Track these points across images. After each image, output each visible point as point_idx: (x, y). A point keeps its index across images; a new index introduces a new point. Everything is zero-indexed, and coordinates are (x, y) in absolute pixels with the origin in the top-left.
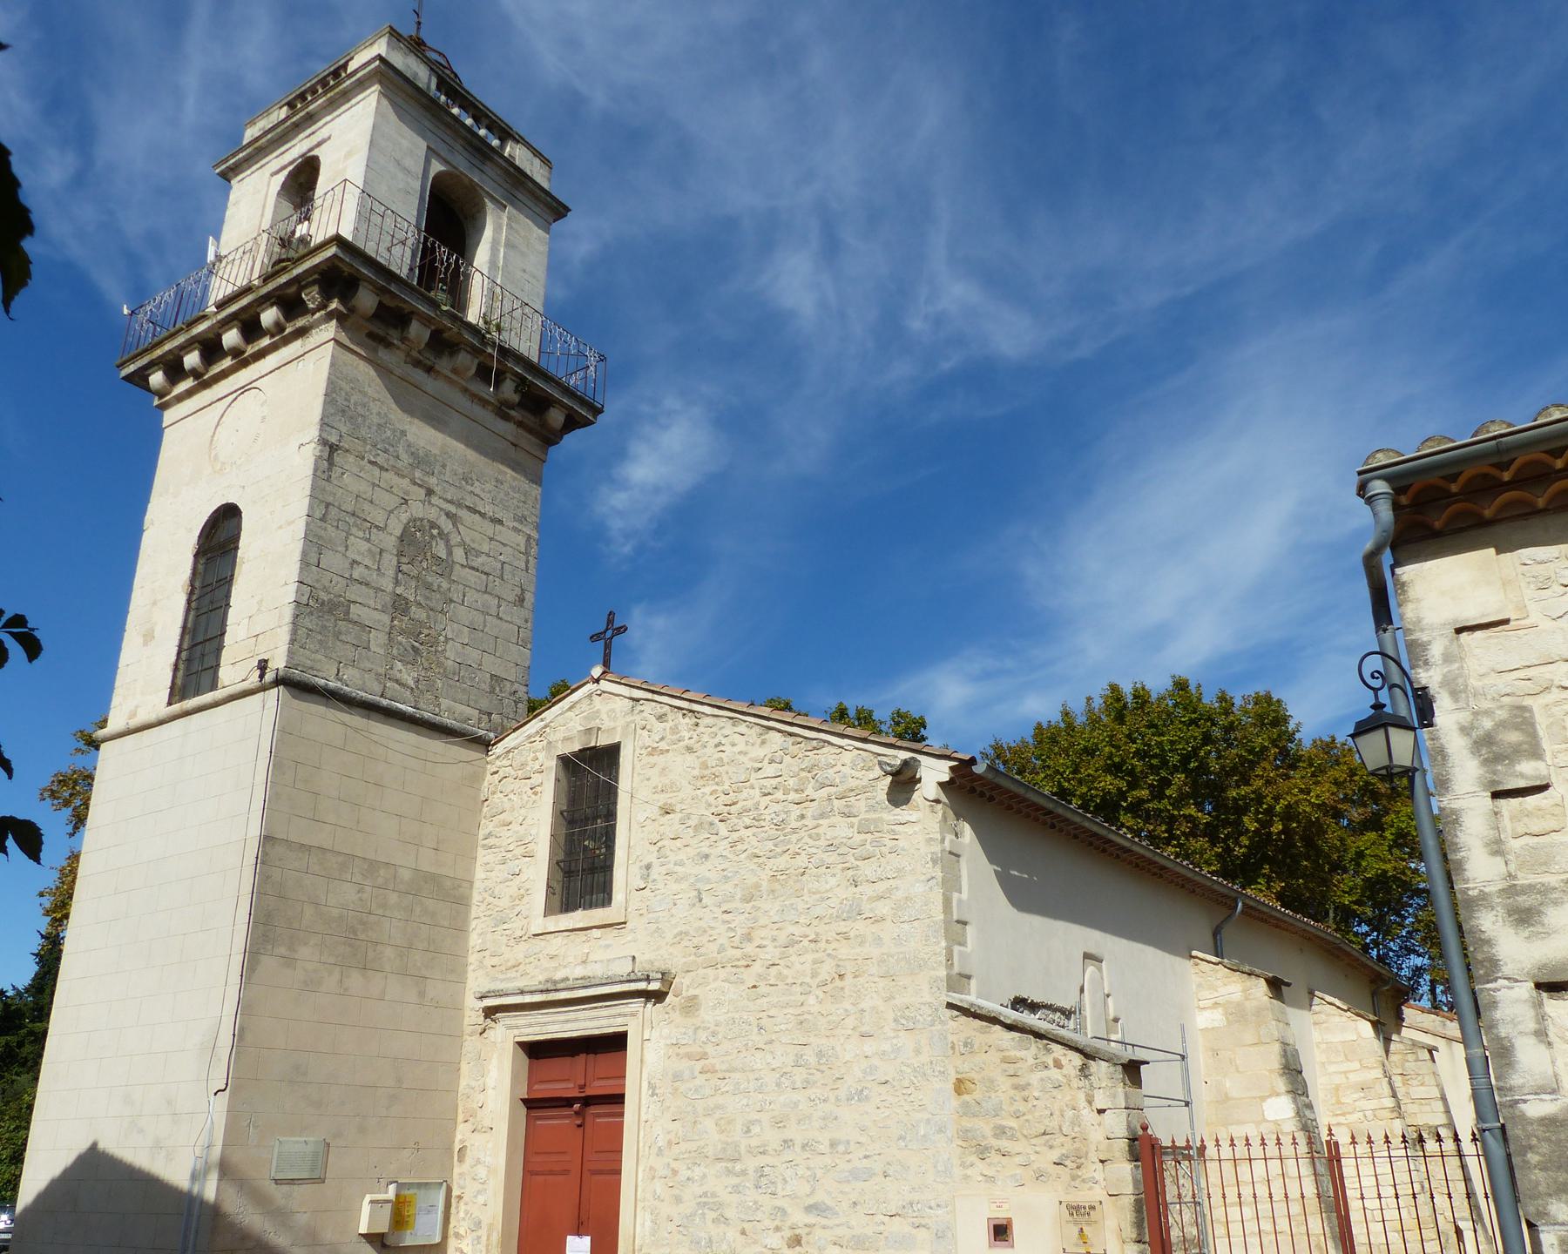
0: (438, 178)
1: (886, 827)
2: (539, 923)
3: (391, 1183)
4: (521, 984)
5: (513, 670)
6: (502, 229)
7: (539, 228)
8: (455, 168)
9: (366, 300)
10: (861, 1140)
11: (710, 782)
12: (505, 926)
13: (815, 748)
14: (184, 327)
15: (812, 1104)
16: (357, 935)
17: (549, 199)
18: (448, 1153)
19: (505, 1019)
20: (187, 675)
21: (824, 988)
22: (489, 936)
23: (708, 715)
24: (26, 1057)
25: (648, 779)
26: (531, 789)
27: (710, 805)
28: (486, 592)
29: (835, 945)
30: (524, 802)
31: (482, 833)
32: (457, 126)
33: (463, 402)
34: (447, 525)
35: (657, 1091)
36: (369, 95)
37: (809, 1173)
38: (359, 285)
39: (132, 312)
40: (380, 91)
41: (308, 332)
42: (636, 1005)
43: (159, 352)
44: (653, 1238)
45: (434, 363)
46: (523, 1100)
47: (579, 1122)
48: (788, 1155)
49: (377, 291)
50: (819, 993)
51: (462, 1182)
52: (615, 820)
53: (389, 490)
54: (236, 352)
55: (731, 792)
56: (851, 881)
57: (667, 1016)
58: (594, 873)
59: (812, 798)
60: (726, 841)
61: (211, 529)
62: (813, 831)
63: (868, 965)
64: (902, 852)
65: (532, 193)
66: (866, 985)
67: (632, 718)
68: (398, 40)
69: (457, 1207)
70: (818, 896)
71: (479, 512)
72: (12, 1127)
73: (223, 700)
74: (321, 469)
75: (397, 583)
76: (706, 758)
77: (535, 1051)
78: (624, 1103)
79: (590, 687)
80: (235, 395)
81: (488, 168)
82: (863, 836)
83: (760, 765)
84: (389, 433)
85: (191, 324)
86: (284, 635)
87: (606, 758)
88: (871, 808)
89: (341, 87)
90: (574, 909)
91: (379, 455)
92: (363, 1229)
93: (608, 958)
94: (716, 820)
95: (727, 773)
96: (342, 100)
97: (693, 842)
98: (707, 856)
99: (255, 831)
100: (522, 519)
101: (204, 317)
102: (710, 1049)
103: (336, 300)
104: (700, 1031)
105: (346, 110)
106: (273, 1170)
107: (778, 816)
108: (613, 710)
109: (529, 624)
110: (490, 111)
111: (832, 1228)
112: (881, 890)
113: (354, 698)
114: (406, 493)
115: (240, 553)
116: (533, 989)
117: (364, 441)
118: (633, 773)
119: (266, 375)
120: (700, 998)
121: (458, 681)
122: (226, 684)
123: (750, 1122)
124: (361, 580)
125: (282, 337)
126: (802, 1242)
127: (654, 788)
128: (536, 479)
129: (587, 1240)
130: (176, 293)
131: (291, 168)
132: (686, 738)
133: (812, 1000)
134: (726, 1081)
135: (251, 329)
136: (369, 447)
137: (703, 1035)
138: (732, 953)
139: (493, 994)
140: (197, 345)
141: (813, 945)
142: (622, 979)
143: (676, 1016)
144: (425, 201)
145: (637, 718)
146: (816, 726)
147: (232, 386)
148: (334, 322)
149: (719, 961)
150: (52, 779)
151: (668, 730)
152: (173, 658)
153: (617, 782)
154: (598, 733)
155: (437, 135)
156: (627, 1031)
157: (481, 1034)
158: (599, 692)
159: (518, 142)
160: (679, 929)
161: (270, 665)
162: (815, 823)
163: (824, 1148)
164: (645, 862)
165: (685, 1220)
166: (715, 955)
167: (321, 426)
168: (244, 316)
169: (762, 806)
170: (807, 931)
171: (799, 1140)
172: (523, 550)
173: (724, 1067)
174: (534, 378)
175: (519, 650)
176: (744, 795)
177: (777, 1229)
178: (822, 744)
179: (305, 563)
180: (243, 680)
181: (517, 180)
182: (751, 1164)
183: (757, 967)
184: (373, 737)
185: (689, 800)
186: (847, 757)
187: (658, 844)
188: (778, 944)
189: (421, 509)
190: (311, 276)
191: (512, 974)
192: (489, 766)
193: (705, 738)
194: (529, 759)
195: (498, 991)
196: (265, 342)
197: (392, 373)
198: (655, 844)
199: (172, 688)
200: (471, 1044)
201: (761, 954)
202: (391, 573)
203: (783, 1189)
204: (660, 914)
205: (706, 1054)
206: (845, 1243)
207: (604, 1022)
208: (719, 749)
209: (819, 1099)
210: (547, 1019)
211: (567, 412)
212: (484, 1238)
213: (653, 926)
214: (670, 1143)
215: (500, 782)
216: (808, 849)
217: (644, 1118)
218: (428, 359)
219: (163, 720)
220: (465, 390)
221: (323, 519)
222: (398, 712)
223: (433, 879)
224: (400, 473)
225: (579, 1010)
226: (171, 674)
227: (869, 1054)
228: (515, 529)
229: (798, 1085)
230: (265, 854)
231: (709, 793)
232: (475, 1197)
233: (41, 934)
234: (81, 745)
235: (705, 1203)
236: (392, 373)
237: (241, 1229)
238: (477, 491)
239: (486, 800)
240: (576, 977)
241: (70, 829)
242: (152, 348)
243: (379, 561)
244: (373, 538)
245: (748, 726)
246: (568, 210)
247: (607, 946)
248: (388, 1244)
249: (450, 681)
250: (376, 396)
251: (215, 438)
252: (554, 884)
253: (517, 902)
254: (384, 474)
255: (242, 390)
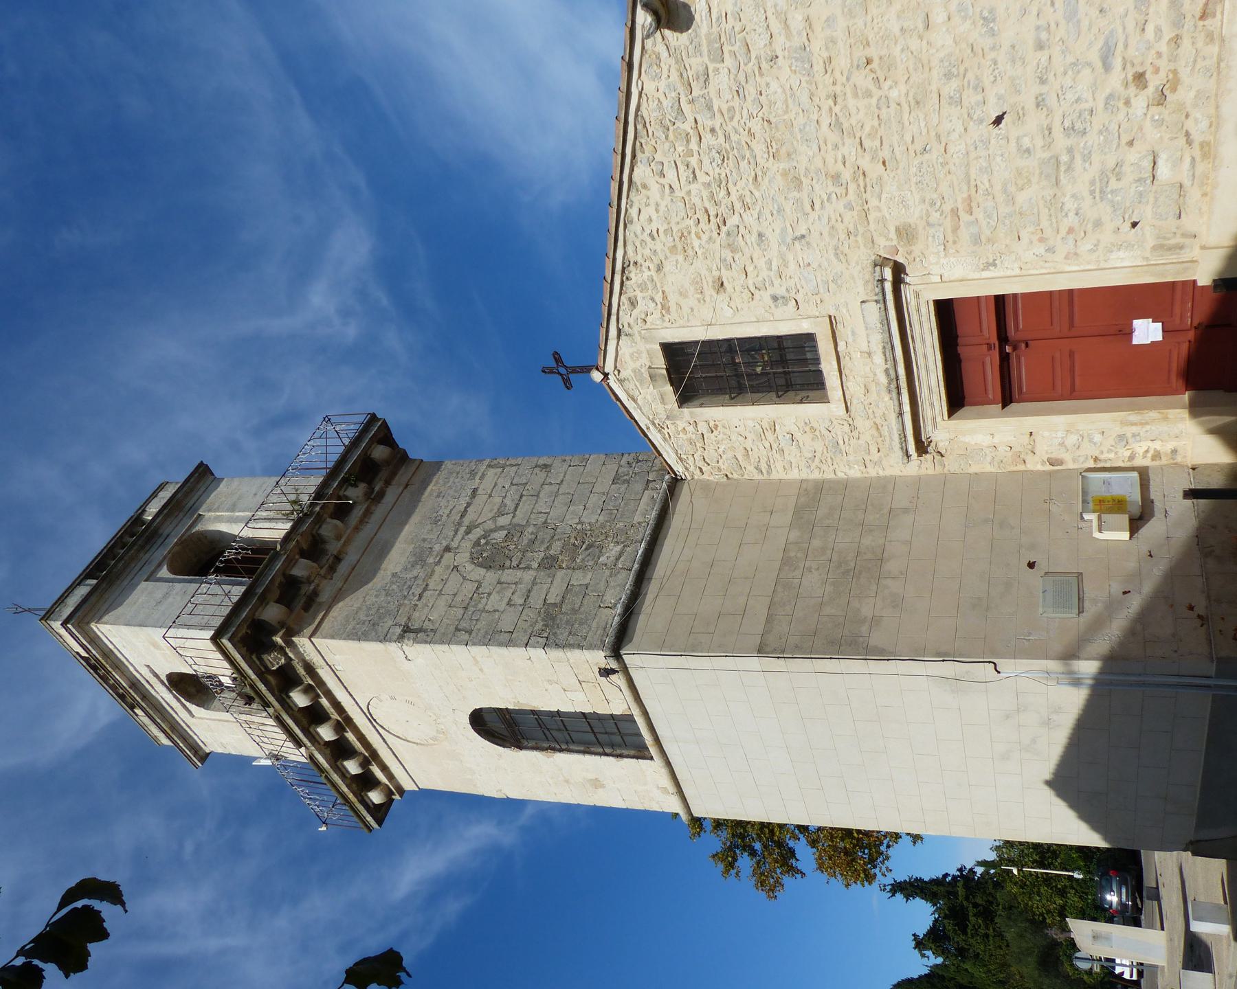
0: (172, 570)
1: (715, 29)
2: (835, 407)
3: (1082, 518)
4: (893, 417)
5: (609, 467)
6: (219, 516)
7: (218, 486)
8: (165, 558)
9: (272, 613)
10: (1035, 13)
11: (689, 241)
12: (841, 442)
13: (645, 126)
14: (324, 775)
15: (999, 78)
16: (851, 570)
17: (192, 480)
18: (1055, 474)
19: (927, 430)
20: (625, 745)
21: (882, 80)
22: (851, 458)
23: (625, 252)
24: (986, 902)
25: (692, 310)
26: (712, 432)
27: (710, 238)
28: (538, 496)
29: (837, 74)
30: (725, 437)
31: (757, 477)
32: (125, 558)
33: (368, 530)
34: (478, 532)
35: (991, 261)
36: (102, 632)
37: (1070, 73)
38: (258, 620)
39: (324, 823)
40: (96, 623)
41: (309, 663)
42: (908, 293)
43: (351, 796)
44: (1136, 247)
45: (332, 555)
46: (1003, 407)
47: (1023, 345)
48: (1052, 101)
49: (264, 605)
50: (886, 85)
51: (1082, 459)
52: (733, 339)
53: (444, 581)
54: (339, 728)
55: (696, 216)
56: (771, 63)
57: (917, 259)
58: (787, 360)
59: (694, 123)
60: (744, 216)
61: (493, 736)
62: (726, 116)
63: (855, 30)
64: (739, 5)
65: (187, 494)
66: (876, 29)
67: (637, 335)
68: (53, 613)
69: (1105, 461)
70: (790, 101)
71: (466, 508)
72: (1038, 898)
73: (640, 707)
74: (425, 637)
75: (528, 568)
76: (666, 249)
77: (956, 401)
78: (1003, 295)
79: (612, 382)
80: (378, 727)
81: (166, 530)
82: (726, 55)
83: (667, 187)
84: (394, 587)
85: (321, 769)
86: (576, 655)
87: (675, 353)
88: (697, 48)
89: (100, 659)
90: (819, 373)
91: (413, 593)
92: (1125, 535)
93: (864, 328)
94: (724, 229)
95: (678, 223)
96: (112, 657)
97: (747, 252)
98: (760, 235)
99: (754, 663)
100: (473, 473)
101: (311, 757)
102: (947, 208)
103: (274, 638)
104: (931, 220)
105: (120, 651)
106: (1071, 615)
107: (714, 159)
108: (632, 355)
109: (567, 458)
110: (117, 534)
111: (1127, 37)
112: (779, 25)
113: (632, 591)
114: (447, 567)
115: (511, 707)
116: (896, 403)
117: (400, 605)
118: (688, 326)
119: (354, 699)
120: (898, 224)
121: (618, 510)
122: (627, 707)
123: (1019, 149)
124: (526, 597)
125: (317, 687)
126: (1141, 71)
127: (699, 302)
128: (437, 465)
129: (1137, 323)
130: (300, 786)
131: (183, 700)
132: (649, 273)
133: (894, 94)
134: (979, 184)
135: (314, 716)
136: (406, 602)
137: (935, 216)
138: (852, 196)
139: (904, 444)
140: (338, 763)
141: (839, 100)
142: (883, 309)
143: (917, 249)
144: (195, 579)
145: (636, 329)
146: (622, 125)
147: (370, 730)
148: (294, 639)
149: (861, 208)
150: (760, 891)
151: (644, 294)
152: (611, 759)
153: (697, 342)
154: (654, 368)
155: (136, 575)
156: (934, 301)
157: (942, 456)
158: (616, 373)
159: (144, 511)
160: (832, 256)
161: (603, 666)
162: (718, 115)
163: (1043, 56)
164: (770, 302)
165: (1118, 213)
166: (855, 213)
167: (387, 641)
168: (305, 722)
169: (707, 179)
170: (825, 109)
171: (1036, 89)
172: (500, 470)
173: (965, 188)
174: (342, 472)
175: (590, 463)
176: (696, 200)
177: (1127, 103)
178: (639, 118)
179: (509, 643)
180: (621, 690)
181: (174, 507)
182: (1061, 142)
183: (865, 163)
184: (668, 573)
185: (708, 262)
186: (650, 87)
187: (753, 289)
188: (841, 142)
189: (463, 555)
190: (254, 662)
191: (885, 431)
192: (696, 477)
193: (647, 252)
194: (685, 437)
195: (901, 439)
196: (324, 702)
197: (340, 589)
198: (753, 295)
199: (637, 758)
200: (952, 465)
201: (851, 160)
202: (519, 573)
203: (1087, 101)
204: (819, 280)
205: (952, 210)
206: (1141, 18)
207: (929, 350)
208: (656, 235)
209: (994, 70)
210: (925, 387)
211: (376, 444)
212: (1135, 429)
213: (832, 286)
214: (1041, 240)
215: (709, 465)
216: (744, 120)
217: (1017, 272)
218: (328, 560)
219: (666, 762)
220: (357, 529)
221: (470, 632)
222: (645, 554)
223: (798, 512)
224: (429, 574)
225: (915, 355)
226: (626, 760)
227: (945, 15)
228: (482, 478)
229: (980, 97)
230: (775, 651)
231: (699, 241)
232: (1095, 444)
233: (892, 896)
234: (733, 872)
235: (1100, 192)
236: (340, 589)
237: (1124, 636)
238: (447, 511)
239: (726, 475)
240: (884, 361)
241: (799, 876)
242: (349, 803)
243: (509, 584)
244: (487, 591)
245: (631, 206)
246: (201, 464)
247: (853, 333)
248: (1139, 514)
249: (619, 516)
250: (361, 600)
251: (418, 741)
252: (799, 398)
253: (817, 433)
254: (430, 587)
255: (372, 720)
